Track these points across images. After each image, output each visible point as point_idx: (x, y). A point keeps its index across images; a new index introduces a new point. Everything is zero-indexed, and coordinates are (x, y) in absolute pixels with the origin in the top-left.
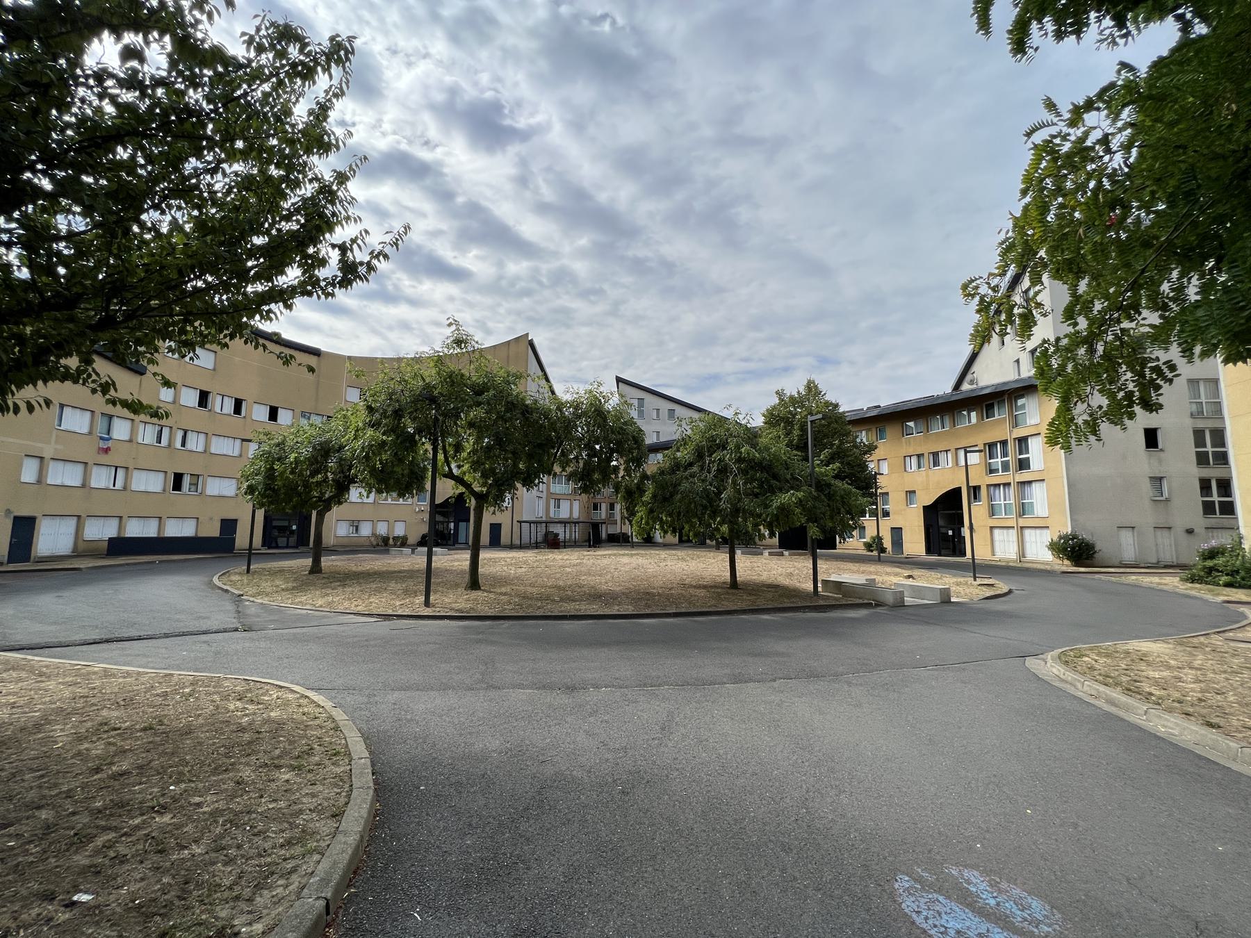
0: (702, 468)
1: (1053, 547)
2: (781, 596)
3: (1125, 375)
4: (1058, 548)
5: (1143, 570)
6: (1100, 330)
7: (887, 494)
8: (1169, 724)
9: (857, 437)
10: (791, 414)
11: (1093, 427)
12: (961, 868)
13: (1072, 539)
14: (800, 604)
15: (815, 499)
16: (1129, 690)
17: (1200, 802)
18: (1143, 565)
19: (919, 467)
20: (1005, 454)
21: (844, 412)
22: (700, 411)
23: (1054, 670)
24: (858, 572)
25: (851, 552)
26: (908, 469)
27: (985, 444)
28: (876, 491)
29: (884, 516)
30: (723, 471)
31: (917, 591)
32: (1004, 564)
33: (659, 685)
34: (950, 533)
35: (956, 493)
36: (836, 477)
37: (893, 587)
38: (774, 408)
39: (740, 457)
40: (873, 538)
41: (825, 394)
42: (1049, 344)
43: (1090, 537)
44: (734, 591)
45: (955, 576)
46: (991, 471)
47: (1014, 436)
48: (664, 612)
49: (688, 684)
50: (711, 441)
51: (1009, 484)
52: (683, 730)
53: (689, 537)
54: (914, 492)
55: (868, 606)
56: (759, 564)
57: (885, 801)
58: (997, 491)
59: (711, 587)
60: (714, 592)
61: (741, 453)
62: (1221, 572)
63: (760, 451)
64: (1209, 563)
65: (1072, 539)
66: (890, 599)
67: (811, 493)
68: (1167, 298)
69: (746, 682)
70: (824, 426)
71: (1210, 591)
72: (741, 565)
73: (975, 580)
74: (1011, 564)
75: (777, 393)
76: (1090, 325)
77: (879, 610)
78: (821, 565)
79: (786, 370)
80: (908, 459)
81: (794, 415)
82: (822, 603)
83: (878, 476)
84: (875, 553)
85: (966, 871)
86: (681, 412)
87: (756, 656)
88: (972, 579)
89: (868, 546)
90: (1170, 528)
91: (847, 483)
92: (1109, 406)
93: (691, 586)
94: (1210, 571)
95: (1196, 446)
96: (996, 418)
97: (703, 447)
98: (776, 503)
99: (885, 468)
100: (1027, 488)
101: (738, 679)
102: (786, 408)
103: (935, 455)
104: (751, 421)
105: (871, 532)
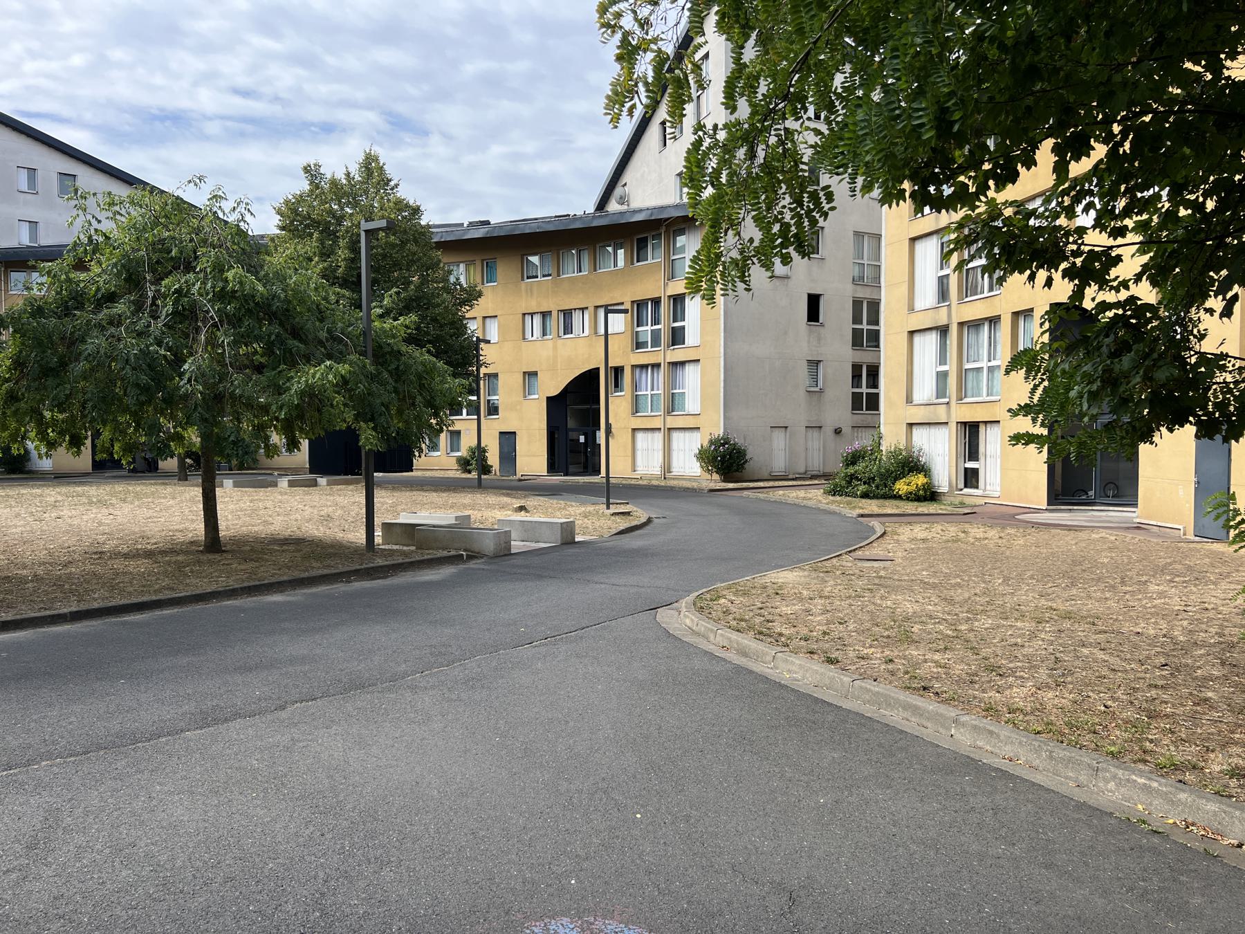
0: (138, 307)
1: (704, 456)
2: (306, 557)
3: (784, 198)
4: (708, 458)
5: (791, 483)
6: (763, 125)
7: (496, 376)
8: (794, 668)
9: (450, 272)
10: (334, 217)
11: (742, 267)
12: (547, 920)
13: (723, 445)
14: (341, 569)
15: (372, 378)
16: (761, 633)
17: (810, 752)
18: (791, 477)
19: (544, 334)
20: (656, 321)
21: (429, 226)
22: (131, 184)
23: (688, 622)
24: (444, 506)
25: (428, 474)
26: (528, 335)
27: (633, 302)
28: (478, 370)
29: (490, 414)
30: (186, 315)
31: (530, 530)
32: (645, 483)
33: (29, 763)
34: (582, 439)
35: (592, 375)
36: (410, 340)
37: (496, 527)
38: (300, 199)
39: (223, 289)
40: (472, 450)
41: (397, 186)
42: (705, 133)
43: (742, 441)
44: (211, 556)
45: (583, 503)
46: (639, 345)
47: (669, 293)
48: (48, 613)
49: (99, 748)
50: (160, 251)
51: (658, 365)
52: (80, 839)
53: (112, 454)
54: (535, 374)
55: (456, 559)
56: (269, 504)
57: (451, 859)
58: (644, 376)
59: (163, 553)
60: (169, 563)
61: (226, 281)
62: (861, 480)
63: (265, 281)
64: (851, 470)
65: (723, 445)
66: (489, 545)
67: (364, 366)
68: (835, 93)
69: (226, 720)
70: (393, 246)
71: (849, 503)
72: (231, 507)
73: (608, 508)
74: (655, 483)
75: (307, 169)
76: (753, 114)
77: (472, 564)
78: (380, 497)
79: (328, 129)
80: (528, 318)
81: (339, 220)
82: (380, 562)
83: (482, 345)
84: (474, 475)
85: (553, 922)
86: (88, 179)
87: (250, 670)
88: (605, 506)
89: (464, 464)
90: (820, 427)
91: (429, 352)
92: (762, 241)
93: (116, 555)
94: (852, 478)
95: (854, 323)
96: (649, 262)
97: (139, 262)
98: (297, 385)
99: (493, 332)
100: (679, 372)
101: (206, 719)
102: (324, 202)
103: (567, 314)
104: (248, 218)
105: (468, 441)
